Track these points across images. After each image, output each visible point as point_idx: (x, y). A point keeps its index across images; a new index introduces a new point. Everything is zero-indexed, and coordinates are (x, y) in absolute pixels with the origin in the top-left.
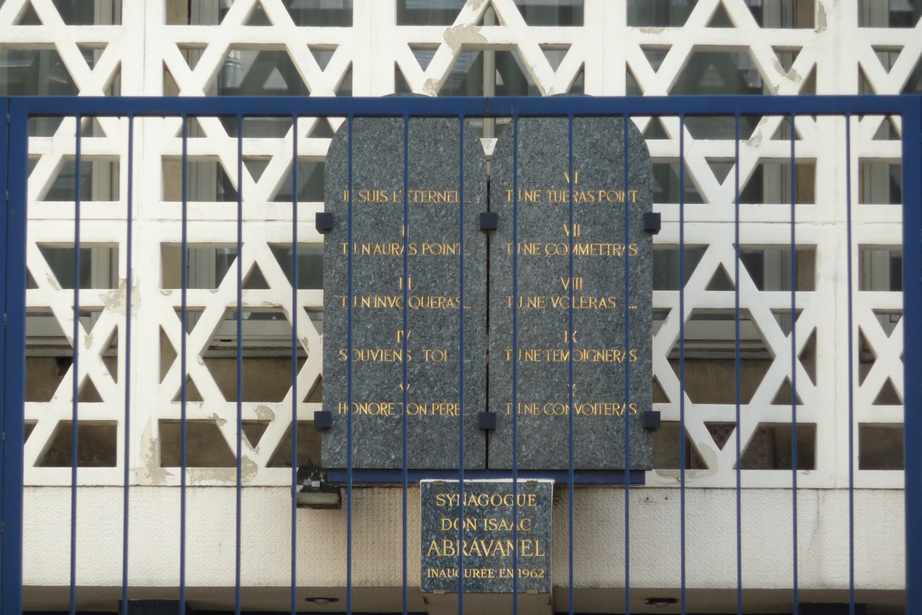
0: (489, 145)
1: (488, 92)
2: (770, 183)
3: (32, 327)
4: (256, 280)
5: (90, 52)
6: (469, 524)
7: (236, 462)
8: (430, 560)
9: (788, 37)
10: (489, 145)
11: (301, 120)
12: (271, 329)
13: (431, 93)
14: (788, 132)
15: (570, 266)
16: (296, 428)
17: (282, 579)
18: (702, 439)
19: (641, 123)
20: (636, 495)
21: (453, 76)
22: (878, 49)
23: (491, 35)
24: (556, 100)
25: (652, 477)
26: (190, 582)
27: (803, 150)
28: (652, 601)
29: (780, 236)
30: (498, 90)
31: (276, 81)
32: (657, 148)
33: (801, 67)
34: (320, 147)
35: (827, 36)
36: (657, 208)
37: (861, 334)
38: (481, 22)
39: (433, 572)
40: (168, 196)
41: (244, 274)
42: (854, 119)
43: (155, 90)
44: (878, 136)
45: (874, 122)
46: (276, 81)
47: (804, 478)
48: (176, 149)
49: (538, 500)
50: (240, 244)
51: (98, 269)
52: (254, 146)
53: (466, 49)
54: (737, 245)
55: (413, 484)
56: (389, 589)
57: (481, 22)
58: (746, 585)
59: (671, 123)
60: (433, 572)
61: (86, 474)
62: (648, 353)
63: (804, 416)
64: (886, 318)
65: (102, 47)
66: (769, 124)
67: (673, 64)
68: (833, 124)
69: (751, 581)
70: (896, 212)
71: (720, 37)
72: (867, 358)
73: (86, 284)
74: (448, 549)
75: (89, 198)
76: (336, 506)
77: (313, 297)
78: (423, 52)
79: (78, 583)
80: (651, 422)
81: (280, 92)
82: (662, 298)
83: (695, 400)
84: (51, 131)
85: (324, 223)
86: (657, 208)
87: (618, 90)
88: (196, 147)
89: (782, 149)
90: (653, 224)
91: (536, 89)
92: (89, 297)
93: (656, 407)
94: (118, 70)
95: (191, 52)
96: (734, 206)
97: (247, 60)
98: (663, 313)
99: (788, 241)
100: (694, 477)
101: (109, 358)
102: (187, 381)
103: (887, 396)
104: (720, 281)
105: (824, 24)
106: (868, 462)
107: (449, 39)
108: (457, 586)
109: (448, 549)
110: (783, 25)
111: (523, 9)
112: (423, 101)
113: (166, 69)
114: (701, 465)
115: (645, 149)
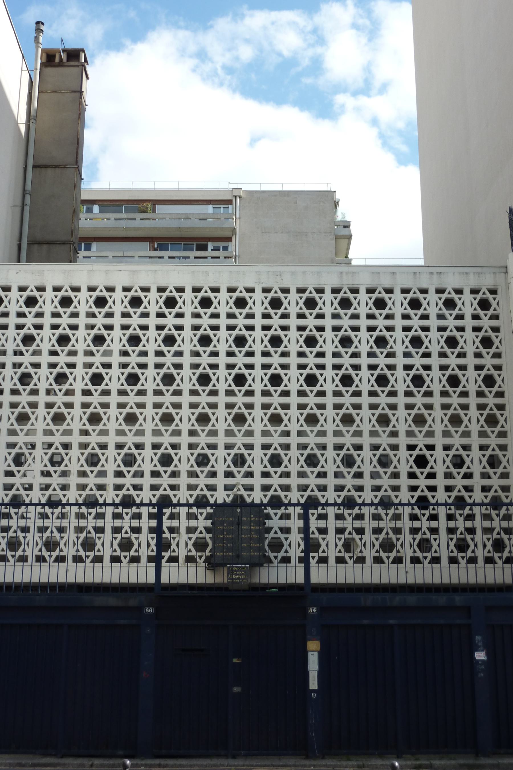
0: (239, 511)
1: (239, 502)
2: (284, 517)
3: (163, 540)
4: (424, 533)
5: (175, 496)
6: (235, 573)
7: (196, 562)
8: (228, 579)
9: (286, 493)
10: (239, 511)
11: (319, 507)
12: (204, 540)
13: (229, 502)
14: (360, 509)
15: (251, 530)
16: (207, 557)
17: (203, 581)
18: (273, 559)
19: (263, 507)
20: (261, 568)
21: (233, 499)
22: (301, 495)
23: (239, 493)
24: (249, 503)
25: (265, 565)
26: (297, 582)
27: (362, 512)
28: (265, 585)
29: (359, 526)
30: (240, 502)
31: (205, 500)
32: (265, 511)
33: (288, 498)
34: (212, 511)
35: (292, 493)
36: (265, 521)
37: (485, 543)
38: (237, 491)
39: (229, 580)
40: (76, 519)
41: (421, 531)
42: (370, 507)
43: (74, 502)
44: (322, 509)
45: (374, 507)
46: (205, 500)
47: (25, 564)
48: (410, 512)
49: (246, 568)
50: (439, 527)
51: (176, 531)
52: (90, 510)
53: (235, 495)
54: (464, 527)
55: (226, 566)
56: (135, 583)
57: (237, 491)
58: (346, 583)
59: (342, 507)
60: (229, 580)
61: (61, 564)
62: (264, 544)
63: (364, 555)
64: (153, 538)
65: (177, 495)
66: (357, 508)
67: (268, 498)
68: (478, 507)
69: (330, 582)
70: (156, 521)
71: (276, 493)
72: (374, 546)
73: (174, 533)
74: (230, 577)
75: (174, 519)
76: (214, 570)
77: (211, 535)
78: (80, 495)
79: (121, 582)
80: (264, 556)
81: (205, 502)
82: (266, 536)
83: (496, 553)
84: (57, 508)
85: (212, 523)
86: (265, 521)
87: (259, 502)
88: (81, 511)
89: (359, 512)
90: (265, 523)
91: (502, 501)
92: (62, 535)
93: (265, 553)
94: (216, 499)
95: (191, 496)
96: (446, 522)
97: (200, 496)
98: (266, 538)
99: (394, 526)
100: (271, 565)
101: (65, 545)
102: (414, 550)
103: (302, 552)
104: (350, 533)
105: (292, 491)
106: (299, 562)
107: (232, 493)
108: (233, 583)
109: (230, 577)
110: (286, 491)
111: (244, 489)
112: (228, 504)
113: (187, 498)
114: (273, 563)
115: (263, 511)
